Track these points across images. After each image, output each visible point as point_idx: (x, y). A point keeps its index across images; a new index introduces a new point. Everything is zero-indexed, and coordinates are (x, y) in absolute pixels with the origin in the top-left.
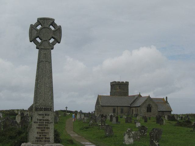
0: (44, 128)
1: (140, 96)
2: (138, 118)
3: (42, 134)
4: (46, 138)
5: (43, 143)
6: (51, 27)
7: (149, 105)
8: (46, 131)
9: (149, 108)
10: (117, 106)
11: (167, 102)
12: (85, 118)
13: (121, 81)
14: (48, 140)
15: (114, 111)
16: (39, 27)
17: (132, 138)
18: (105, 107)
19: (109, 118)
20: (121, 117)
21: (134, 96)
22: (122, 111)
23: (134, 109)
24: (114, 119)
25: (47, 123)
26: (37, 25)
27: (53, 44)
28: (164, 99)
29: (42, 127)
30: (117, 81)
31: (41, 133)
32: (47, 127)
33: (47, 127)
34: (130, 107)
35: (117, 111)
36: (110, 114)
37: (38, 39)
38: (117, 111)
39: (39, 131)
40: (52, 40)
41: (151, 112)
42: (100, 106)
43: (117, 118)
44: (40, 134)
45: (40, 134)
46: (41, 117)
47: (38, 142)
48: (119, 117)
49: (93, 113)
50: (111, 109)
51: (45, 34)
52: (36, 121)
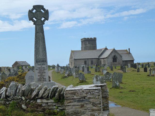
0: (42, 72)
1: (106, 49)
2: (105, 67)
3: (41, 77)
4: (43, 79)
5: (42, 81)
6: (42, 10)
7: (115, 56)
8: (44, 74)
9: (115, 59)
10: (88, 59)
11: (130, 53)
12: (62, 70)
13: (90, 37)
14: (45, 80)
15: (85, 63)
16: (34, 11)
17: (99, 81)
18: (78, 60)
19: (81, 69)
20: (91, 68)
21: (101, 50)
22: (92, 63)
23: (102, 60)
24: (86, 69)
25: (44, 69)
26: (33, 10)
27: (44, 21)
28: (127, 50)
29: (41, 72)
30: (86, 37)
31: (40, 76)
32: (44, 72)
33: (44, 72)
34: (99, 59)
35: (92, 87)
36: (82, 66)
37: (34, 19)
38: (92, 87)
39: (39, 74)
40: (43, 19)
41: (116, 62)
42: (73, 59)
43: (88, 68)
44: (40, 76)
45: (40, 76)
46: (40, 66)
47: (39, 81)
48: (90, 67)
49: (68, 66)
50: (83, 61)
51: (39, 15)
52: (37, 68)
